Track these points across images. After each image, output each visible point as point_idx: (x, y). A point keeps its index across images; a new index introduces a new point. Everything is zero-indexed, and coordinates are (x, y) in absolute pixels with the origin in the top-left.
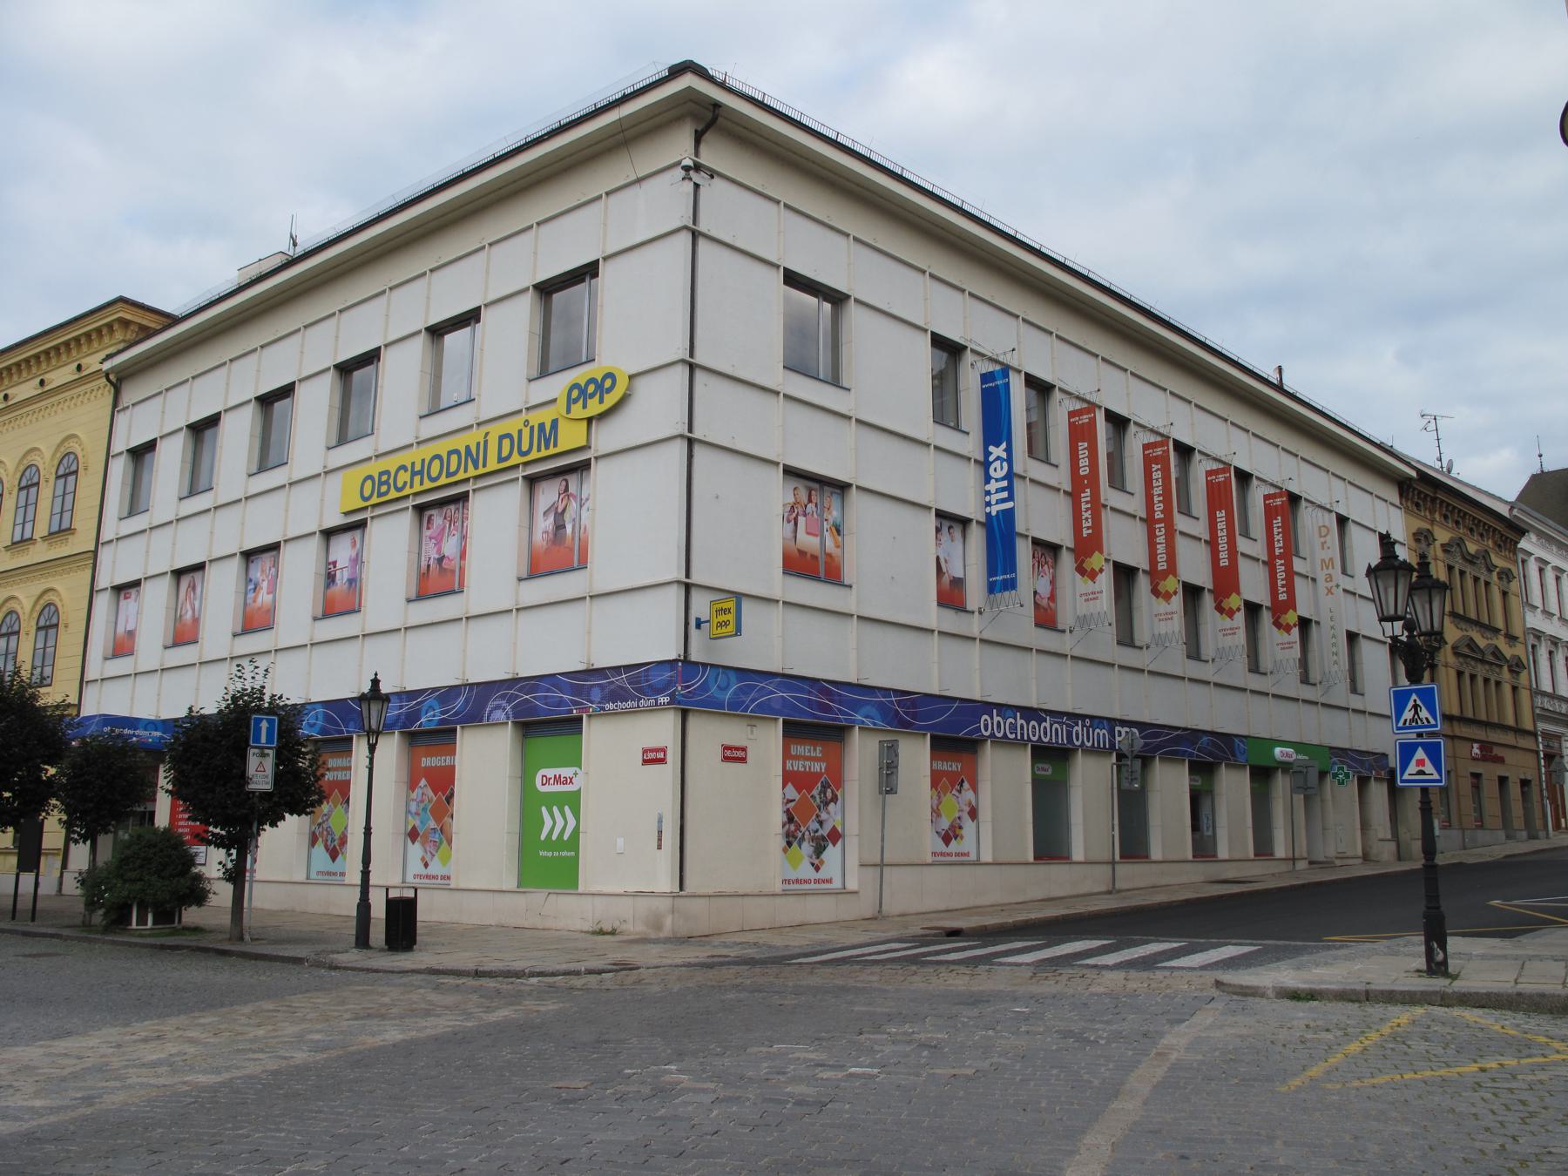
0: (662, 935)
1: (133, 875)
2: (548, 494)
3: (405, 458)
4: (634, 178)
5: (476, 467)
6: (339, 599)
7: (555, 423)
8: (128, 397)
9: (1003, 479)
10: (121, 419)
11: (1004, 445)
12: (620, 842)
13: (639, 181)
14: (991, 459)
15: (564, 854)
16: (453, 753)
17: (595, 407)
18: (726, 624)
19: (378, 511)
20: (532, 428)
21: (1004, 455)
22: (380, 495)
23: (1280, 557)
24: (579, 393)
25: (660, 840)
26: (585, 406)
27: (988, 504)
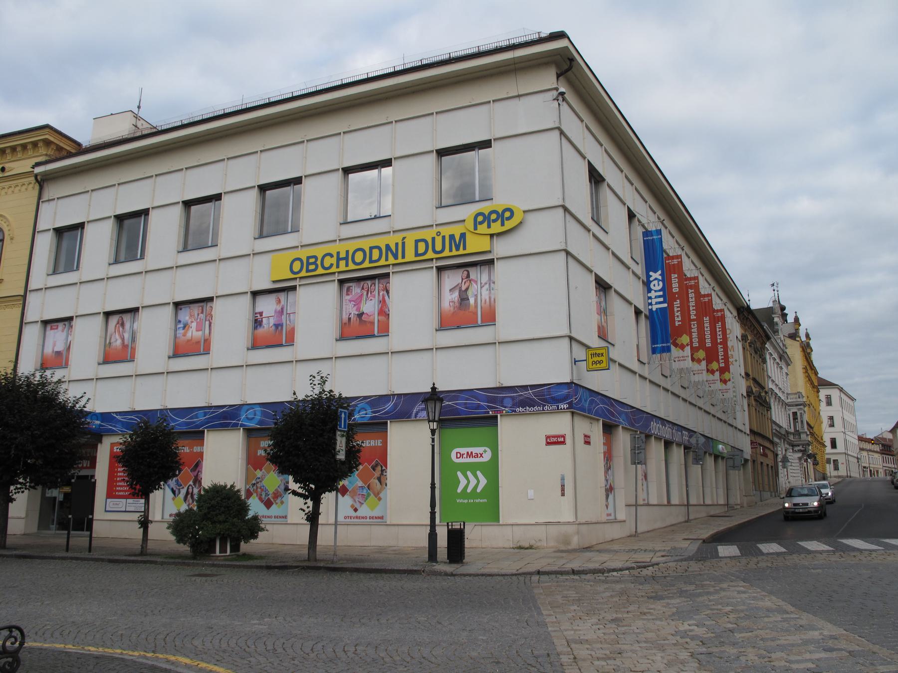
0: (570, 548)
1: (222, 518)
2: (452, 279)
3: (333, 249)
4: (516, 94)
5: (396, 257)
6: (269, 337)
7: (463, 236)
8: (47, 194)
9: (660, 291)
10: (44, 207)
11: (660, 272)
12: (531, 493)
13: (519, 96)
14: (651, 279)
15: (477, 501)
16: (203, 445)
17: (496, 228)
18: (600, 362)
19: (304, 282)
20: (444, 237)
21: (660, 278)
22: (308, 271)
23: (721, 343)
24: (485, 218)
25: (563, 490)
26: (489, 227)
27: (651, 304)
